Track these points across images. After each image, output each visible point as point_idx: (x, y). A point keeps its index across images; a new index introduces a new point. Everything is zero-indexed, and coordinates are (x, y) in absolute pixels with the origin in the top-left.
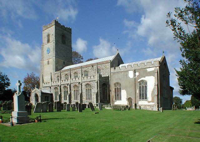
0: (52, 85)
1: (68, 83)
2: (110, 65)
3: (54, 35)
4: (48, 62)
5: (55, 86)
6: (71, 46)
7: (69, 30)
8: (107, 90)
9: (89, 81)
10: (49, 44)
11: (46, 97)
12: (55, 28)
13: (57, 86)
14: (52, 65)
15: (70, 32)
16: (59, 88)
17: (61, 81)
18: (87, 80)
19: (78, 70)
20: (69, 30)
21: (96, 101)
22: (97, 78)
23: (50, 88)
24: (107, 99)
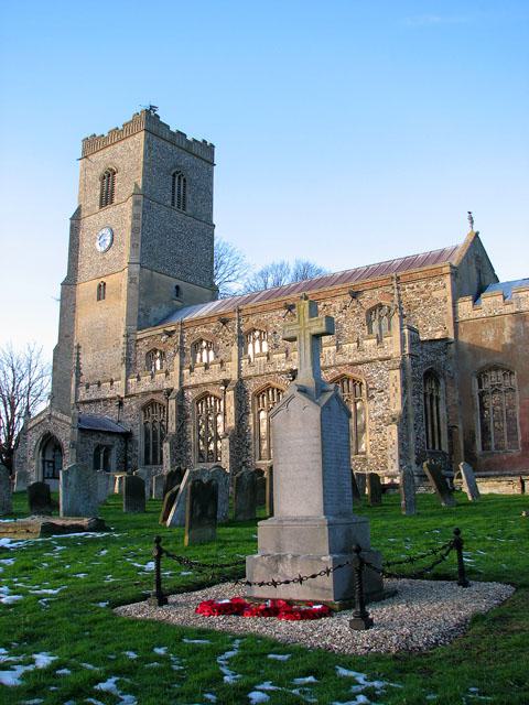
0: (131, 391)
1: (223, 376)
2: (449, 287)
3: (141, 170)
4: (102, 288)
5: (145, 394)
6: (210, 215)
7: (203, 154)
8: (442, 403)
9: (352, 364)
10: (110, 210)
11: (98, 449)
12: (147, 141)
13: (160, 398)
14: (123, 304)
15: (208, 158)
16: (172, 403)
17: (186, 371)
18: (340, 359)
19: (266, 316)
20: (203, 154)
21: (396, 457)
22: (394, 347)
23: (121, 404)
24: (440, 448)
